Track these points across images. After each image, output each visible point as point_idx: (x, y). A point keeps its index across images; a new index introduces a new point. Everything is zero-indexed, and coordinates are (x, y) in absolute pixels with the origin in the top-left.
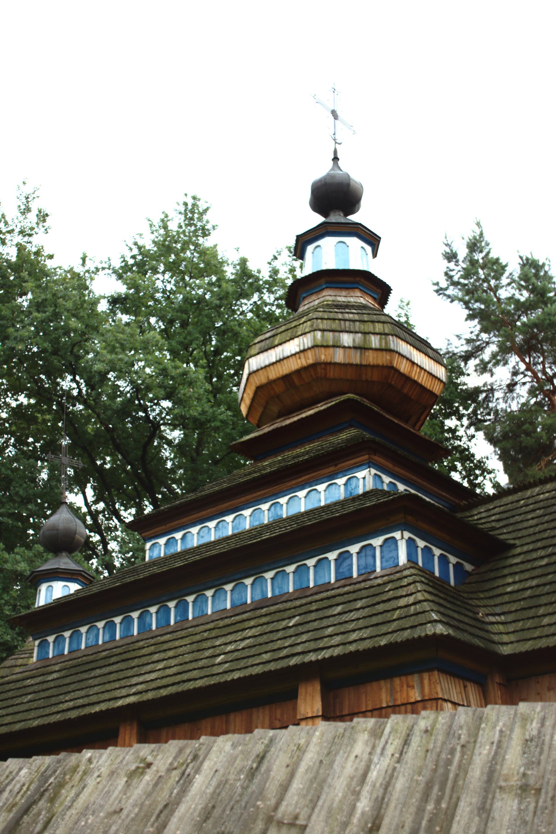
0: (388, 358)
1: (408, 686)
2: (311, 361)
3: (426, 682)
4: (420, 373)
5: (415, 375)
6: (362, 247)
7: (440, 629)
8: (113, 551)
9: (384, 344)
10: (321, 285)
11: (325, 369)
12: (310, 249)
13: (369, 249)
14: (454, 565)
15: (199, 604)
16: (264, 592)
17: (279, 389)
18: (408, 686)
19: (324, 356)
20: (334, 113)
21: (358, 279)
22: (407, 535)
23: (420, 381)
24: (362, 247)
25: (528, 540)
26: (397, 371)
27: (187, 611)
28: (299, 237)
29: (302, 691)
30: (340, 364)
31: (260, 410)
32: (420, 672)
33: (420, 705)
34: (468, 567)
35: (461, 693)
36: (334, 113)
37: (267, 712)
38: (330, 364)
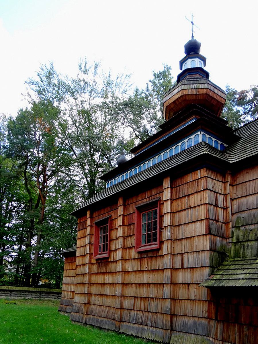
0: (206, 91)
1: (196, 174)
2: (181, 95)
3: (202, 172)
4: (217, 96)
5: (215, 96)
6: (200, 62)
7: (206, 152)
8: (109, 115)
9: (204, 86)
10: (186, 74)
11: (185, 97)
12: (183, 64)
13: (202, 62)
14: (220, 144)
15: (144, 166)
16: (161, 159)
17: (172, 106)
18: (196, 174)
19: (185, 93)
20: (192, 23)
21: (198, 71)
22: (202, 133)
23: (217, 99)
24: (200, 62)
25: (252, 141)
26: (209, 95)
27: (141, 169)
28: (180, 62)
29: (164, 181)
30: (190, 94)
31: (168, 115)
32: (200, 169)
33: (200, 179)
34: (226, 145)
35: (215, 176)
36: (192, 23)
37: (156, 189)
38: (187, 95)
